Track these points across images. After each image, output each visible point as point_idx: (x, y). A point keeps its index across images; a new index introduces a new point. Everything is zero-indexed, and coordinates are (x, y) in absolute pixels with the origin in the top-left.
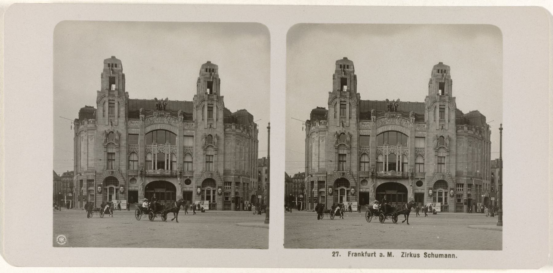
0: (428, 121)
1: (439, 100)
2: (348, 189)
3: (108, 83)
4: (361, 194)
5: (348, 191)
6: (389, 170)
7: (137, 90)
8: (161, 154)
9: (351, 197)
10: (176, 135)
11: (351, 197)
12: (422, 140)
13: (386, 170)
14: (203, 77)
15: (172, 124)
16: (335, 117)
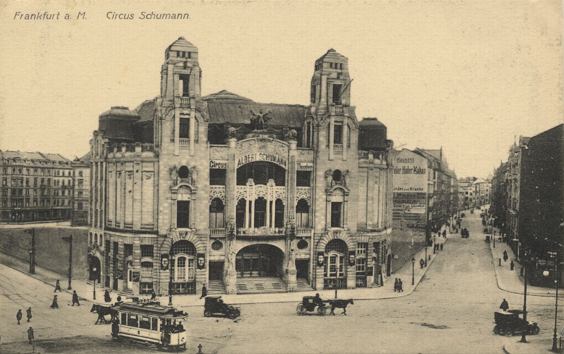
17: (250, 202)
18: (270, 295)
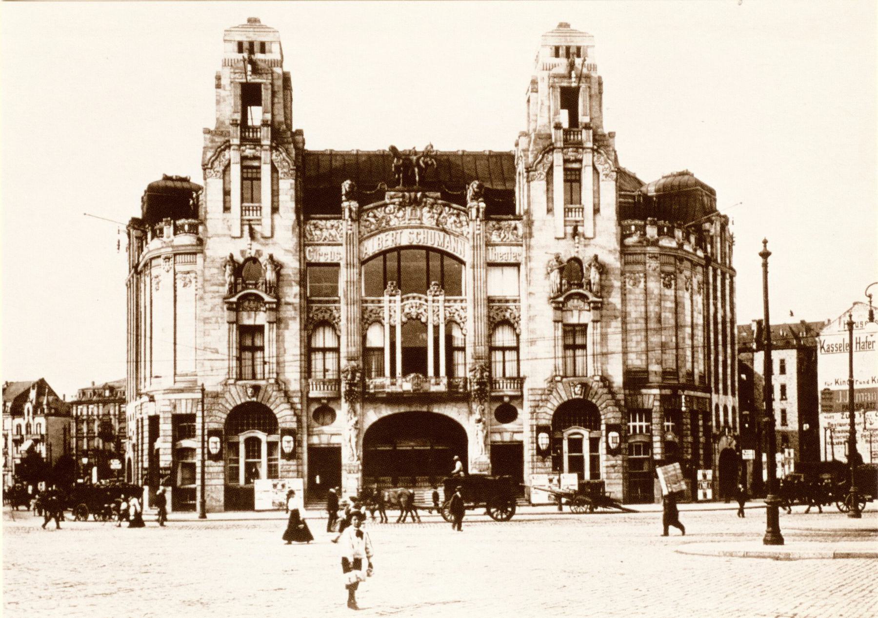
0: (527, 212)
1: (560, 144)
2: (274, 438)
3: (239, 102)
4: (313, 450)
5: (272, 446)
6: (405, 374)
7: (330, 125)
8: (414, 325)
9: (281, 462)
10: (462, 262)
11: (281, 462)
12: (511, 272)
13: (393, 374)
14: (546, 74)
15: (448, 227)
16: (227, 209)
17: (436, 328)
18: (851, 561)
